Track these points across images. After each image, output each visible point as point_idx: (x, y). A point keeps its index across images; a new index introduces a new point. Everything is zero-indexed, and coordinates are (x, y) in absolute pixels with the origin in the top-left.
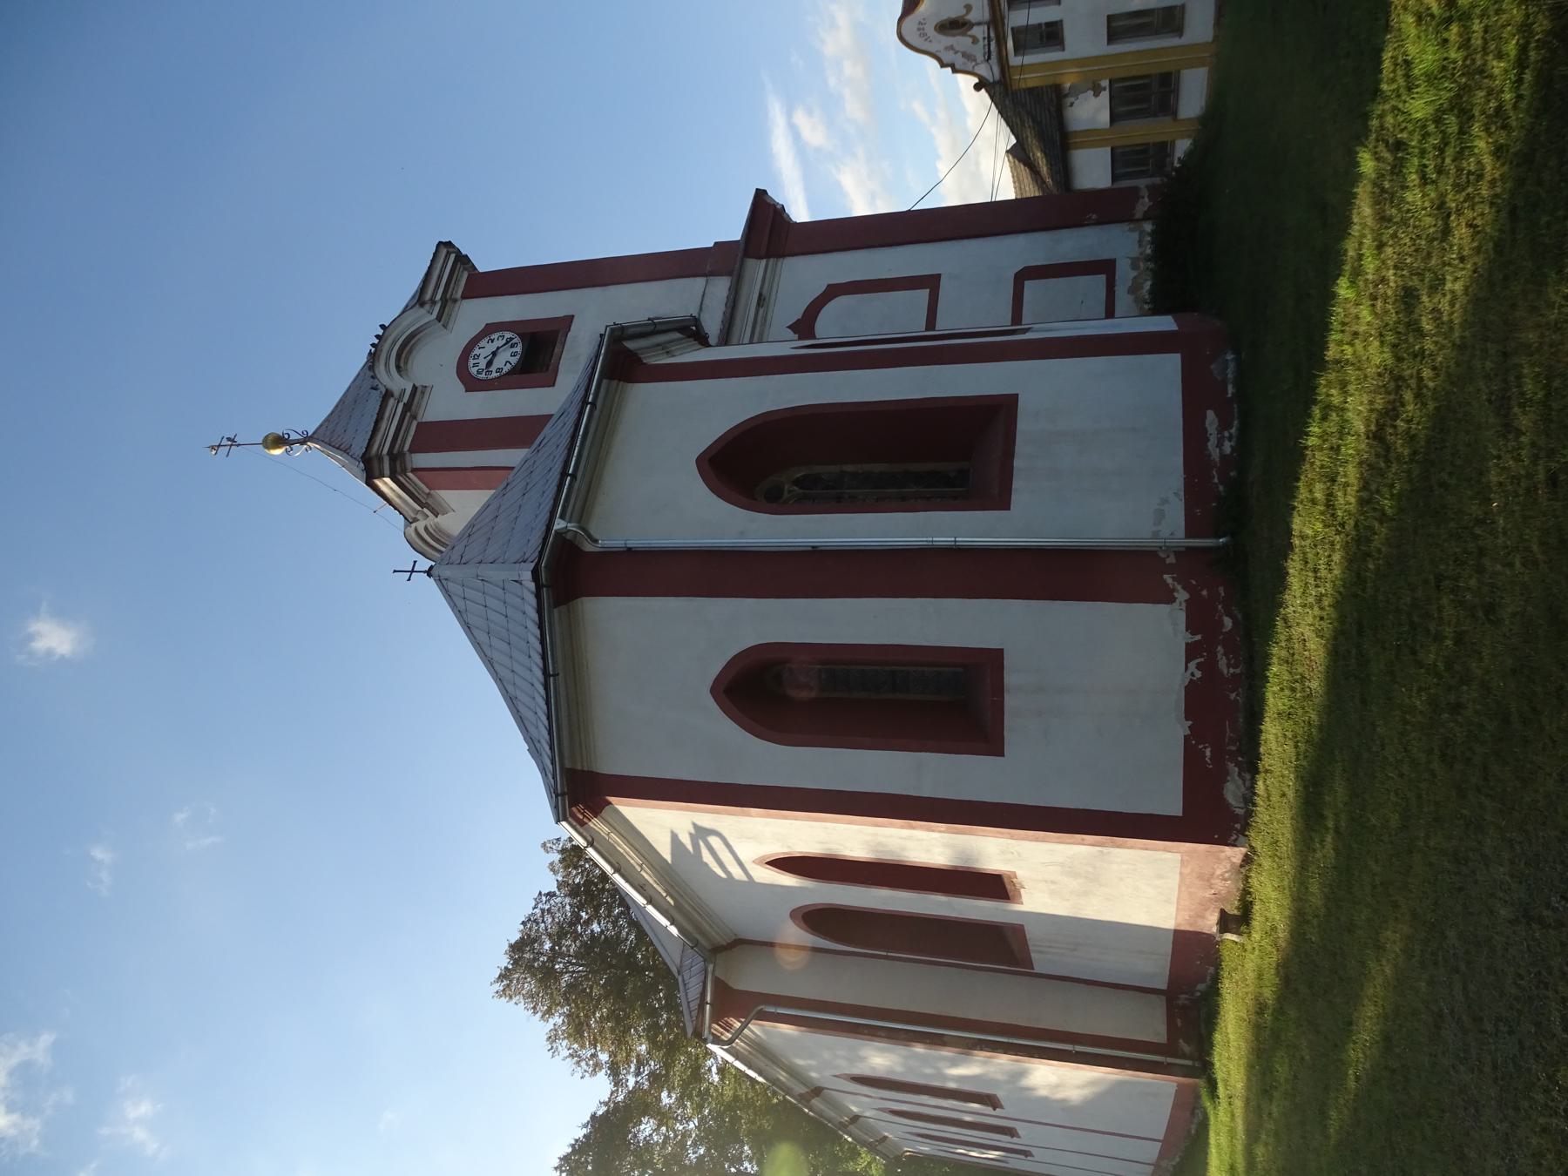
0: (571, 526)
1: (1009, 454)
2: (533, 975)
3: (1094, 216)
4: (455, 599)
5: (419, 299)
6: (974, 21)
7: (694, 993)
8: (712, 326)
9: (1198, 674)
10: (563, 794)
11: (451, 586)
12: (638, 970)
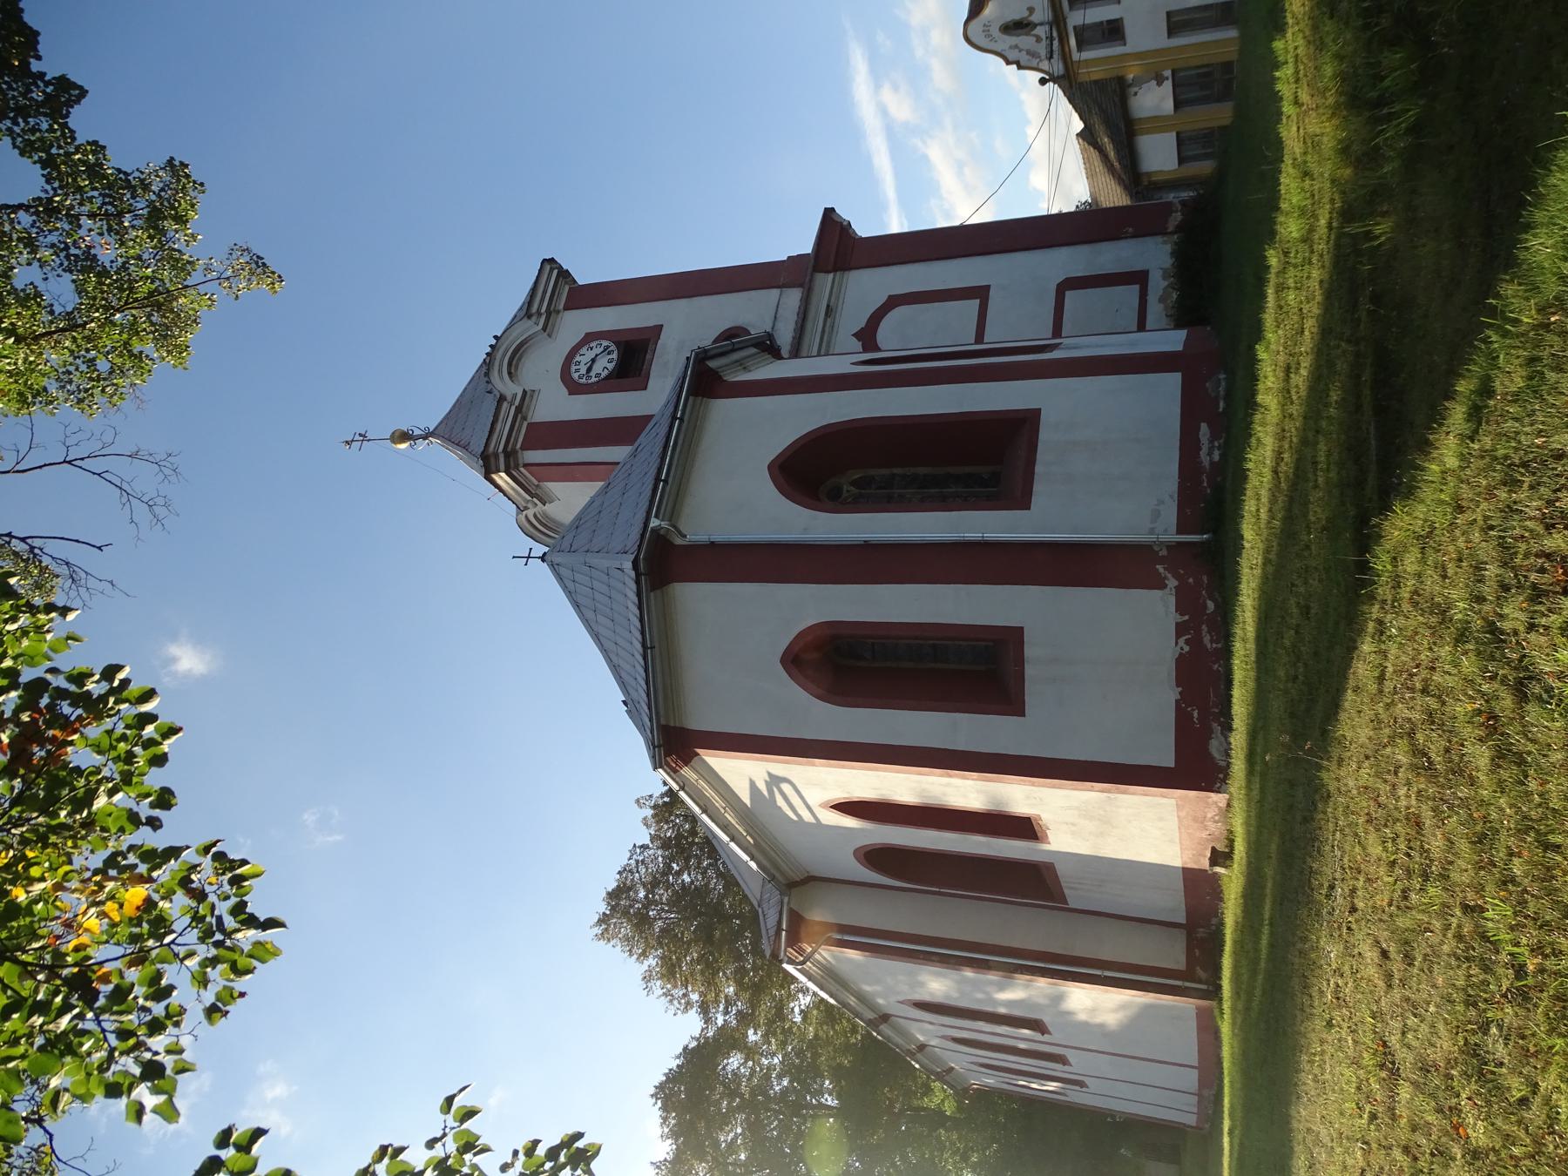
0: (664, 524)
1: (1031, 462)
2: (630, 920)
3: (1131, 229)
4: (566, 581)
5: (527, 311)
6: (1036, 21)
7: (772, 921)
8: (785, 338)
9: (1187, 648)
10: (659, 746)
11: (562, 571)
12: (726, 918)
